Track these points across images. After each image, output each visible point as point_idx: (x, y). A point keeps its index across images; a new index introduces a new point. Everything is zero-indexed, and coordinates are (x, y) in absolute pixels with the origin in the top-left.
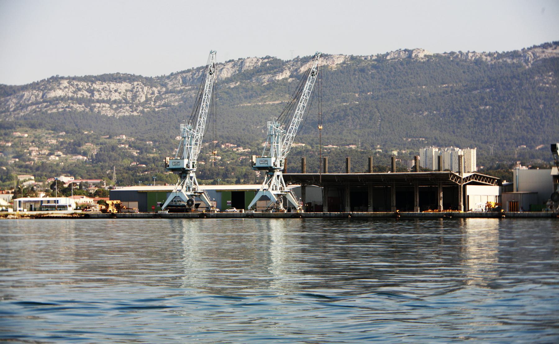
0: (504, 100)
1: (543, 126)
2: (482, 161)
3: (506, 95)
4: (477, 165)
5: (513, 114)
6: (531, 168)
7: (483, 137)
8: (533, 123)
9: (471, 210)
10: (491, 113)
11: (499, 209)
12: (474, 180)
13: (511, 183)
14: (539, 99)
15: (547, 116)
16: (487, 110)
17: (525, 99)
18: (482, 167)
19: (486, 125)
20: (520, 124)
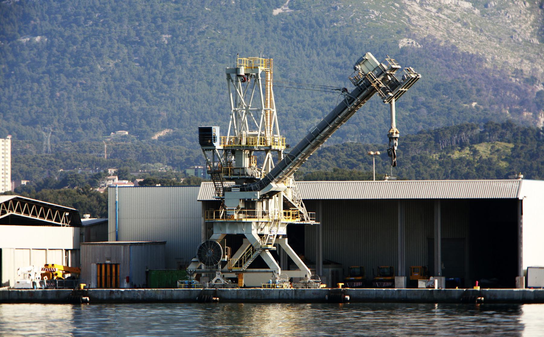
0: (76, 21)
1: (169, 84)
2: (24, 167)
3: (83, 11)
4: (14, 178)
5: (99, 56)
6: (141, 184)
7: (27, 110)
8: (145, 77)
9: (8, 284)
10: (45, 54)
11: (73, 282)
12: (15, 213)
13: (103, 219)
14: (159, 21)
15: (179, 62)
16: (36, 46)
17: (126, 21)
18: (24, 182)
19: (33, 80)
20: (115, 80)
